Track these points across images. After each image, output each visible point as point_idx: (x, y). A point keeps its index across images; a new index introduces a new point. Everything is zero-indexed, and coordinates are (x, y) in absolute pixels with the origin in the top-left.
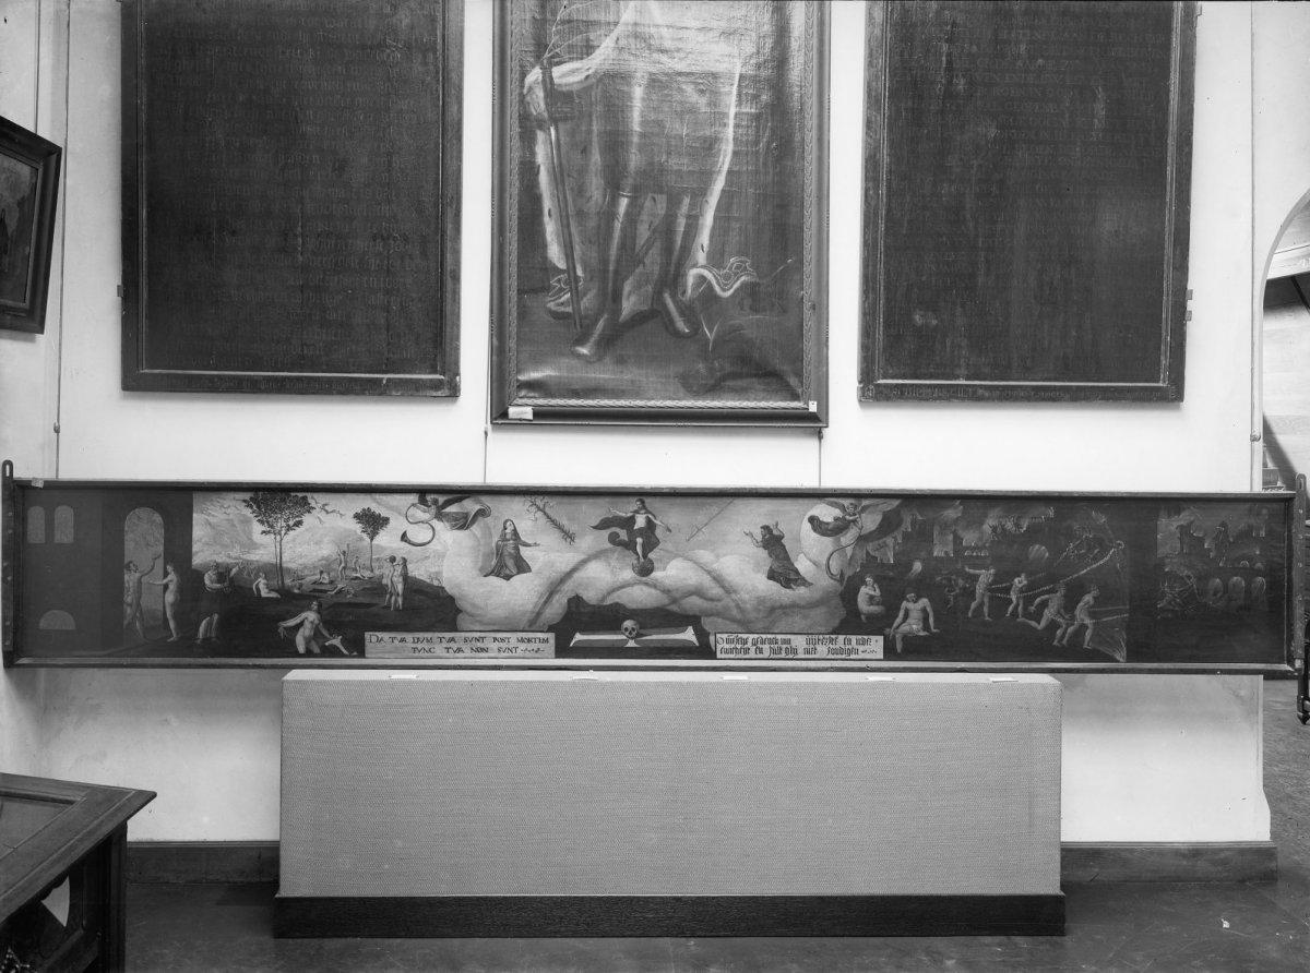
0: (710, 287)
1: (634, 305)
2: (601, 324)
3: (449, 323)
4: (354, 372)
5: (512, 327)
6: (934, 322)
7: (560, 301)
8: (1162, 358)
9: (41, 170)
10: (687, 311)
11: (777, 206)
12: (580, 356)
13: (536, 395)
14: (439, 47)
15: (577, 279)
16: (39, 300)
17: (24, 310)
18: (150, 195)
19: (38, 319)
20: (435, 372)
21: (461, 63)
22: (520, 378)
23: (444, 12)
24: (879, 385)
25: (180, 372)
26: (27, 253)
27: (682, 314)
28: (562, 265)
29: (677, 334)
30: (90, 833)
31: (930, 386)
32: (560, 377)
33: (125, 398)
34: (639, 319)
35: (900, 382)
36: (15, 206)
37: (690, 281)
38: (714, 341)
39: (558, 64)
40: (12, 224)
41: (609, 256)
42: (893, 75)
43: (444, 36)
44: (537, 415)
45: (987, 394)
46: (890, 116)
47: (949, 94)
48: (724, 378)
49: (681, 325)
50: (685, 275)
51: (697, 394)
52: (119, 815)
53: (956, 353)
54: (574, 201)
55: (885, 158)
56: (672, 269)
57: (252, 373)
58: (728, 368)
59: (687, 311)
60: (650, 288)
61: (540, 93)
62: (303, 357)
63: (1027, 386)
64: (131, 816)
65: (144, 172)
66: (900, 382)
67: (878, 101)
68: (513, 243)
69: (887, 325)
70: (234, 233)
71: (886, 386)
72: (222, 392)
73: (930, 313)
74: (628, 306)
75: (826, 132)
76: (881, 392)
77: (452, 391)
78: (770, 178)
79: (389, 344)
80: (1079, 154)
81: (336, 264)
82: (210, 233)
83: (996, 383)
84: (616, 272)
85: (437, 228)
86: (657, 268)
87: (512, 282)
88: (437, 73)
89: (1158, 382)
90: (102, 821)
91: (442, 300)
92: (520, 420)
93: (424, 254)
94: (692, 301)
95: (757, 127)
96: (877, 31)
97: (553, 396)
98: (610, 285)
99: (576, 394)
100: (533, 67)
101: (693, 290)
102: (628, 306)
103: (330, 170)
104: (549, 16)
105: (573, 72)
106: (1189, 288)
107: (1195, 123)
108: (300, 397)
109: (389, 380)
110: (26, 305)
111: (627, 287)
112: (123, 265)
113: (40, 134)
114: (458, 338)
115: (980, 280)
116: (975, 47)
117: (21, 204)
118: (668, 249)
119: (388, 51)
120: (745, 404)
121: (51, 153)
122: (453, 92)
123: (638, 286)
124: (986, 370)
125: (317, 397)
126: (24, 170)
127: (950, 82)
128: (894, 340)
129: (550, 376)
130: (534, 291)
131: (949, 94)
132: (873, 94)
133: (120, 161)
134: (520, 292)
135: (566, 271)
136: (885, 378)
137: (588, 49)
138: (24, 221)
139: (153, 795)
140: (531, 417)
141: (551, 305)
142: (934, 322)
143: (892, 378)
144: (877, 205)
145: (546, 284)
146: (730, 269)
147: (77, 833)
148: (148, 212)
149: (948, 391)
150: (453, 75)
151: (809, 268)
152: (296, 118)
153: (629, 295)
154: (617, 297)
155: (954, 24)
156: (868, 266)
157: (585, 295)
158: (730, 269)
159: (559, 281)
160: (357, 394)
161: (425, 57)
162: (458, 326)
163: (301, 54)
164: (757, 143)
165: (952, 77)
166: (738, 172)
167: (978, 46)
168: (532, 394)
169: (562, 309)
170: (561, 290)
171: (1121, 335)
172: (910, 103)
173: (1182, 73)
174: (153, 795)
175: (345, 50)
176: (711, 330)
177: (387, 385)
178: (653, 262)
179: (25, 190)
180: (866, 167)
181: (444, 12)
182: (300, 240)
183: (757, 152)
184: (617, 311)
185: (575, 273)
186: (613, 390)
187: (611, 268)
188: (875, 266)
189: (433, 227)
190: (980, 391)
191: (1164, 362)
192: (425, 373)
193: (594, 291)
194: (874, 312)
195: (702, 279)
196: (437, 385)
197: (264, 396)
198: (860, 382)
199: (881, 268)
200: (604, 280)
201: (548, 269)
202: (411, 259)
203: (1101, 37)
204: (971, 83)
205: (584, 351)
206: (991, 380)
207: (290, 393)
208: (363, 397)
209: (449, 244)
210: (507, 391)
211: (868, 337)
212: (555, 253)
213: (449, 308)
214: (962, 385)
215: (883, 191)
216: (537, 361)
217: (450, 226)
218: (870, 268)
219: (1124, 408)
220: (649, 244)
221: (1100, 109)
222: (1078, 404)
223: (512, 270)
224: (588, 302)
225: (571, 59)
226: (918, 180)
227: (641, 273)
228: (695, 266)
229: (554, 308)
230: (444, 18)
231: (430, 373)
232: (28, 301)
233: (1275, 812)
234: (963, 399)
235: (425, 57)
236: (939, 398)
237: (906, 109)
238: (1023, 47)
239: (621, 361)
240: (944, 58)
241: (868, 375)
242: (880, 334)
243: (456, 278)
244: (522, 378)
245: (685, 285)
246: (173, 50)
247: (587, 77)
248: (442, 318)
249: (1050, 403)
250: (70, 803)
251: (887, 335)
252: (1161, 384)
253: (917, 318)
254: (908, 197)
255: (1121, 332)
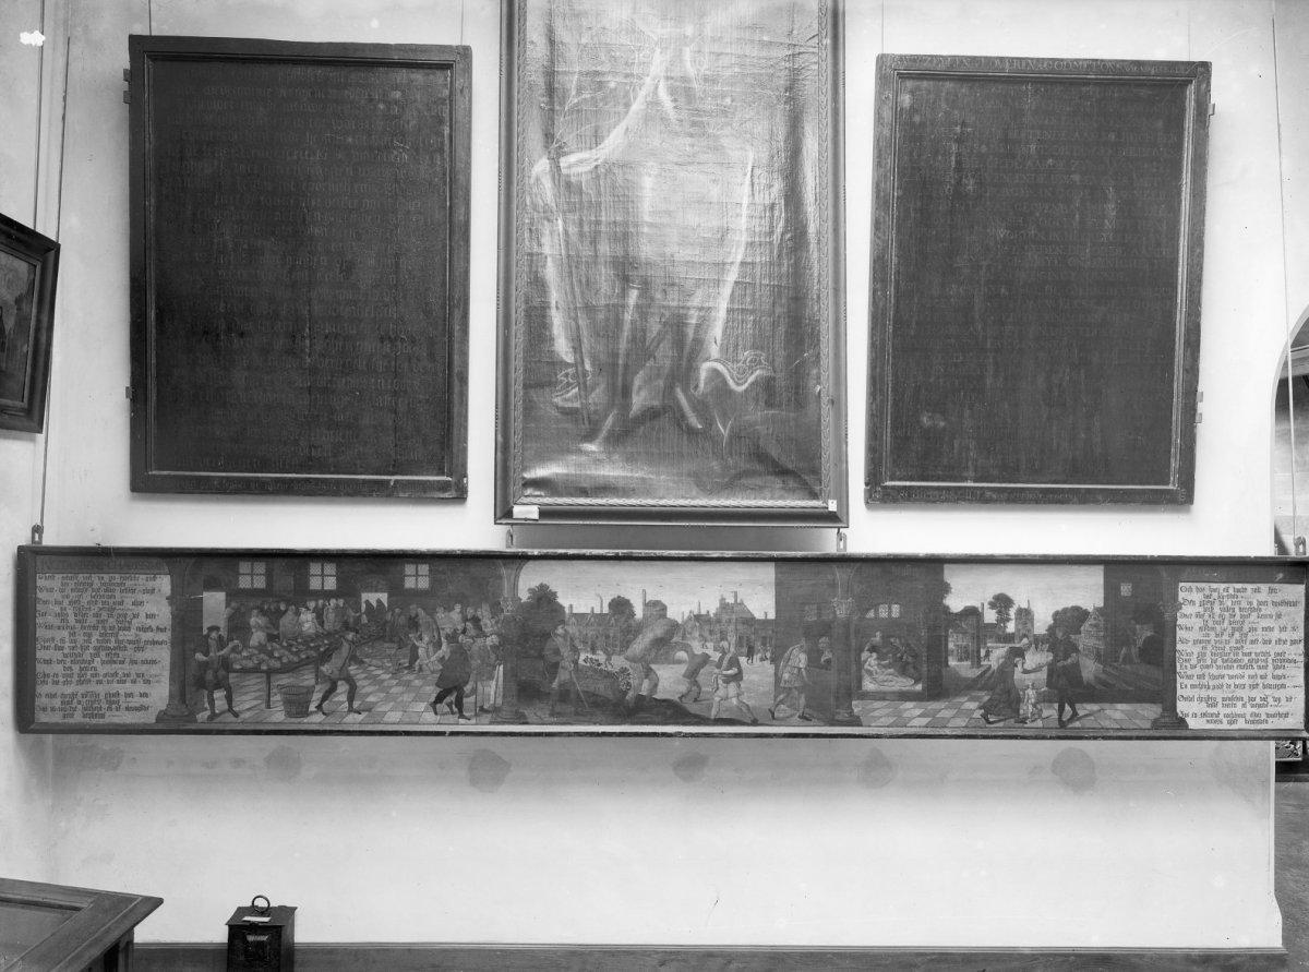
0: (725, 382)
1: (645, 400)
2: (610, 421)
3: (456, 425)
4: (361, 474)
5: (517, 424)
6: (942, 424)
7: (568, 398)
8: (1172, 460)
9: (38, 268)
10: (701, 407)
11: (792, 298)
12: (587, 453)
13: (543, 494)
14: (447, 148)
15: (585, 374)
16: (38, 397)
17: (22, 410)
18: (159, 296)
19: (36, 418)
20: (443, 474)
21: (468, 164)
22: (525, 475)
23: (451, 113)
24: (886, 487)
25: (187, 473)
26: (25, 351)
27: (695, 409)
28: (569, 358)
29: (691, 431)
30: (97, 941)
31: (938, 488)
32: (567, 475)
33: (134, 499)
34: (651, 414)
35: (908, 484)
36: (13, 303)
37: (703, 375)
38: (731, 437)
39: (565, 154)
40: (10, 323)
41: (618, 349)
42: (902, 175)
43: (451, 136)
44: (543, 514)
45: (994, 496)
46: (898, 217)
47: (959, 194)
48: (739, 476)
49: (695, 421)
50: (698, 369)
51: (710, 493)
52: (126, 922)
53: (964, 454)
54: (582, 293)
55: (893, 258)
56: (684, 363)
57: (260, 475)
58: (744, 465)
59: (701, 407)
60: (661, 383)
61: (547, 183)
62: (310, 459)
63: (1036, 489)
64: (138, 923)
65: (152, 274)
66: (908, 484)
67: (886, 202)
68: (519, 336)
69: (895, 428)
70: (242, 335)
71: (893, 488)
72: (230, 493)
73: (938, 416)
74: (639, 400)
75: (842, 224)
76: (888, 495)
77: (460, 496)
78: (784, 269)
79: (396, 446)
80: (1088, 256)
81: (344, 365)
82: (218, 335)
83: (1004, 485)
84: (626, 366)
85: (444, 329)
86: (668, 363)
87: (517, 376)
88: (444, 174)
89: (1168, 484)
90: (109, 928)
91: (450, 402)
92: (526, 519)
93: (431, 356)
94: (705, 395)
95: (772, 217)
96: (886, 132)
97: (560, 495)
98: (620, 379)
99: (584, 492)
100: (540, 157)
101: (706, 384)
102: (639, 400)
103: (338, 271)
104: (557, 108)
105: (581, 161)
106: (1200, 389)
107: (1207, 223)
108: (307, 498)
109: (396, 481)
110: (25, 404)
111: (637, 382)
112: (132, 368)
113: (39, 230)
114: (465, 440)
115: (989, 381)
116: (984, 146)
117: (18, 301)
118: (679, 342)
119: (395, 153)
120: (761, 503)
121: (50, 250)
122: (460, 193)
123: (649, 380)
124: (995, 472)
125: (326, 498)
126: (22, 267)
127: (959, 182)
128: (901, 444)
129: (557, 474)
130: (540, 385)
131: (959, 194)
132: (882, 194)
133: (128, 263)
134: (526, 387)
135: (575, 365)
136: (892, 480)
137: (597, 138)
138: (22, 321)
139: (159, 902)
140: (536, 516)
141: (558, 400)
142: (942, 424)
143: (900, 480)
144: (885, 306)
145: (554, 380)
146: (745, 362)
147: (84, 941)
148: (157, 314)
149: (956, 493)
150: (461, 177)
151: (827, 361)
152: (304, 220)
153: (640, 388)
154: (626, 392)
155: (964, 124)
156: (876, 367)
157: (593, 389)
158: (745, 362)
159: (567, 375)
160: (364, 496)
161: (432, 158)
162: (466, 428)
163: (309, 156)
164: (771, 233)
165: (961, 178)
166: (753, 264)
167: (988, 145)
168: (538, 493)
169: (569, 405)
170: (568, 384)
171: (1131, 437)
172: (919, 204)
173: (1194, 172)
174: (159, 902)
175: (353, 151)
176: (725, 428)
177: (395, 487)
178: (665, 354)
179: (22, 288)
180: (874, 268)
181: (451, 113)
182: (308, 342)
183: (771, 243)
184: (626, 406)
185: (584, 367)
186: (623, 489)
187: (621, 362)
188: (882, 368)
189: (440, 328)
190: (988, 494)
191: (1174, 464)
192: (432, 475)
193: (603, 386)
194: (882, 413)
195: (716, 372)
196: (444, 487)
197: (271, 497)
198: (867, 484)
199: (889, 369)
200: (614, 374)
201: (556, 364)
202: (419, 360)
203: (1112, 137)
204: (980, 184)
205: (591, 447)
206: (1000, 482)
207: (299, 495)
208: (371, 498)
209: (456, 346)
210: (512, 489)
211: (876, 439)
212: (562, 347)
213: (456, 410)
214: (969, 488)
215: (891, 291)
216: (542, 458)
217: (457, 328)
218: (878, 370)
219: (1134, 511)
220: (660, 338)
221: (1111, 209)
222: (1086, 506)
223: (517, 363)
224: (598, 396)
225: (580, 150)
226: (927, 282)
227: (651, 368)
228: (707, 359)
229: (561, 404)
230: (451, 119)
231: (438, 475)
232: (26, 400)
233: (1286, 916)
234: (970, 501)
235: (432, 158)
236: (947, 501)
237: (915, 209)
238: (1033, 147)
239: (630, 459)
240: (953, 158)
241: (875, 475)
242: (887, 437)
243: (464, 380)
244: (528, 475)
245: (697, 379)
246: (181, 152)
247: (596, 167)
248: (449, 419)
249: (1058, 505)
250: (77, 909)
251: (895, 438)
252: (1170, 487)
253: (925, 420)
254: (916, 300)
255: (1130, 434)
